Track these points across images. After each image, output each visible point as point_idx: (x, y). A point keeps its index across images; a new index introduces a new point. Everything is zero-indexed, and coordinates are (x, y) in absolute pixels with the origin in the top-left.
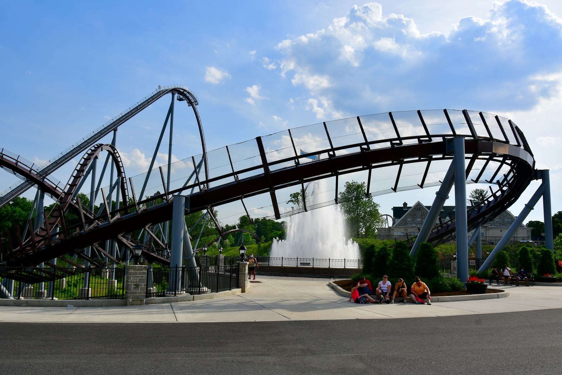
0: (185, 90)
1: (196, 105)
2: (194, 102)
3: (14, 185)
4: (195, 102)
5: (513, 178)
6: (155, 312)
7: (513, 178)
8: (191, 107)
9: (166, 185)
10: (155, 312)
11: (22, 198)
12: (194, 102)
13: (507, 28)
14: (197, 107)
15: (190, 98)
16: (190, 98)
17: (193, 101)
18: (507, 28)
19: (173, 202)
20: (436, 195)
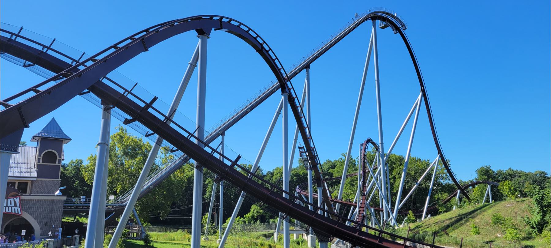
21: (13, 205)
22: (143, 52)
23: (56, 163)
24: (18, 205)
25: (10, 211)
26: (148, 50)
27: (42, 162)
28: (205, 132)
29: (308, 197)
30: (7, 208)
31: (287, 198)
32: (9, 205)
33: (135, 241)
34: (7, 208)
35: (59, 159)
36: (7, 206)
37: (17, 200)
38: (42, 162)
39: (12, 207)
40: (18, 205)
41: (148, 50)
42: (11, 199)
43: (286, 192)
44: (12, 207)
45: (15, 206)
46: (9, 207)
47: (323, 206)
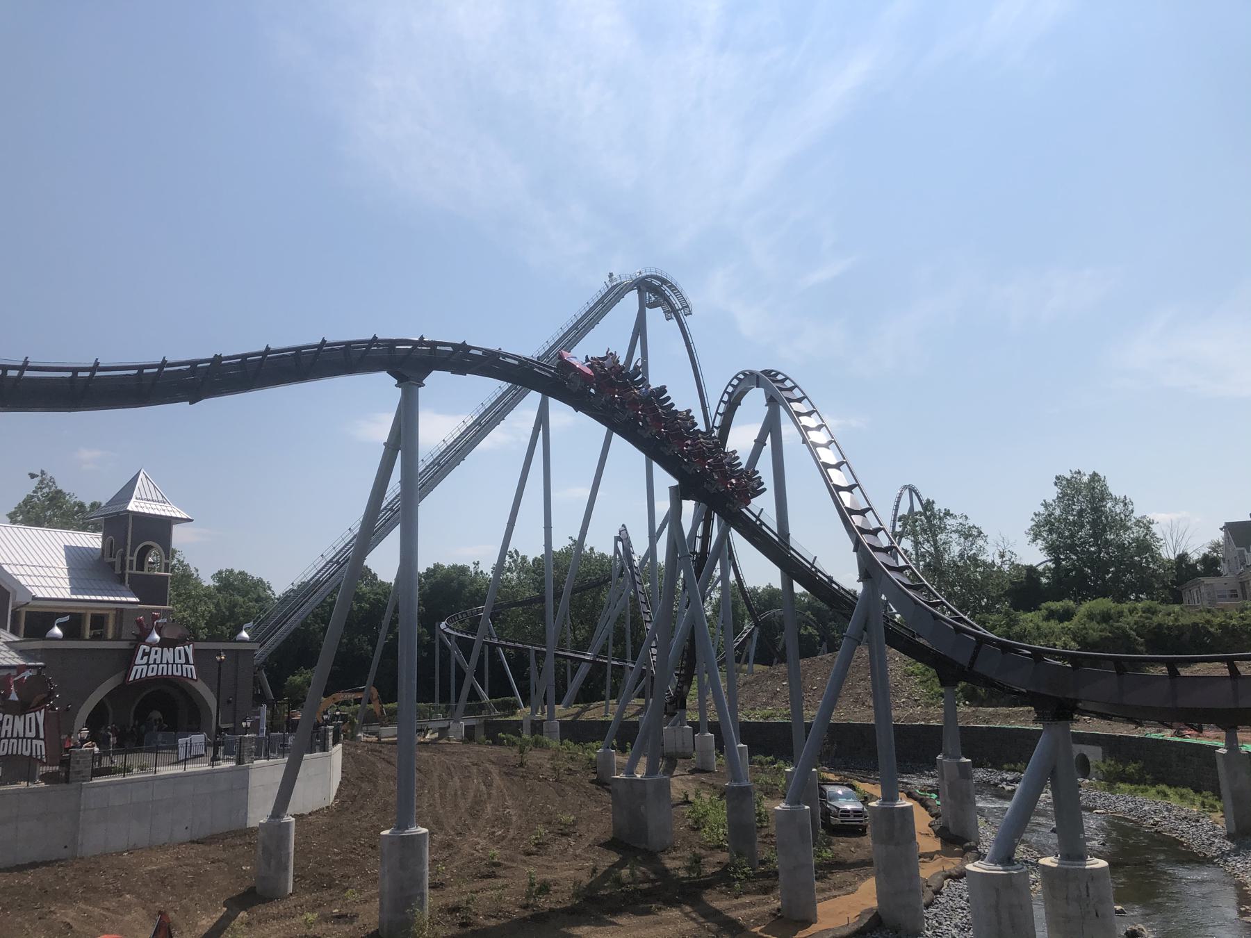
0: (664, 281)
1: (686, 315)
2: (680, 310)
3: (449, 436)
4: (683, 308)
5: (189, 367)
6: (459, 440)
7: (189, 367)
8: (674, 322)
9: (710, 697)
10: (459, 440)
11: (425, 571)
12: (680, 310)
13: (327, 924)
14: (689, 321)
15: (674, 299)
16: (672, 300)
17: (678, 306)
18: (327, 924)
19: (21, 651)
20: (212, 357)
21: (183, 661)
22: (671, 507)
23: (143, 570)
24: (191, 661)
25: (179, 674)
26: (854, 551)
27: (137, 570)
28: (420, 463)
29: (932, 607)
30: (175, 666)
31: (505, 389)
32: (177, 661)
33: (427, 850)
34: (175, 666)
35: (165, 564)
36: (158, 665)
37: (190, 650)
38: (137, 570)
39: (182, 665)
40: (191, 661)
41: (854, 551)
42: (157, 648)
43: (620, 865)
44: (182, 665)
45: (187, 662)
46: (177, 664)
47: (735, 573)
